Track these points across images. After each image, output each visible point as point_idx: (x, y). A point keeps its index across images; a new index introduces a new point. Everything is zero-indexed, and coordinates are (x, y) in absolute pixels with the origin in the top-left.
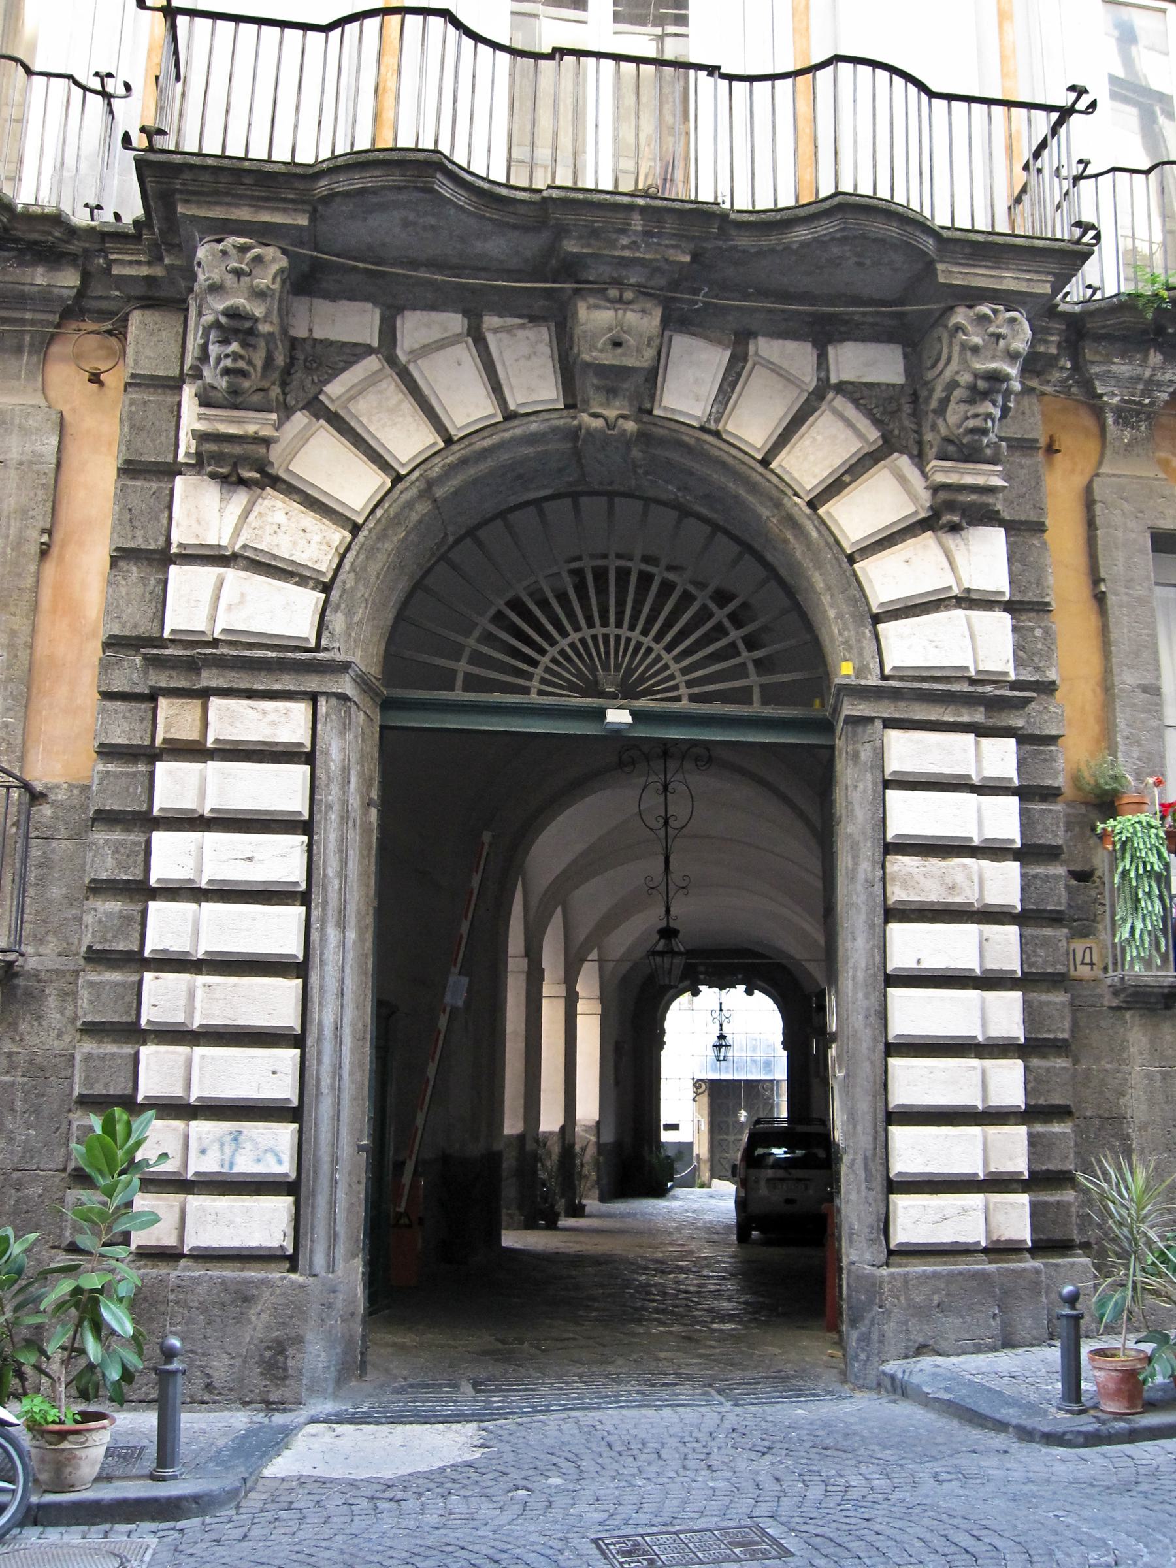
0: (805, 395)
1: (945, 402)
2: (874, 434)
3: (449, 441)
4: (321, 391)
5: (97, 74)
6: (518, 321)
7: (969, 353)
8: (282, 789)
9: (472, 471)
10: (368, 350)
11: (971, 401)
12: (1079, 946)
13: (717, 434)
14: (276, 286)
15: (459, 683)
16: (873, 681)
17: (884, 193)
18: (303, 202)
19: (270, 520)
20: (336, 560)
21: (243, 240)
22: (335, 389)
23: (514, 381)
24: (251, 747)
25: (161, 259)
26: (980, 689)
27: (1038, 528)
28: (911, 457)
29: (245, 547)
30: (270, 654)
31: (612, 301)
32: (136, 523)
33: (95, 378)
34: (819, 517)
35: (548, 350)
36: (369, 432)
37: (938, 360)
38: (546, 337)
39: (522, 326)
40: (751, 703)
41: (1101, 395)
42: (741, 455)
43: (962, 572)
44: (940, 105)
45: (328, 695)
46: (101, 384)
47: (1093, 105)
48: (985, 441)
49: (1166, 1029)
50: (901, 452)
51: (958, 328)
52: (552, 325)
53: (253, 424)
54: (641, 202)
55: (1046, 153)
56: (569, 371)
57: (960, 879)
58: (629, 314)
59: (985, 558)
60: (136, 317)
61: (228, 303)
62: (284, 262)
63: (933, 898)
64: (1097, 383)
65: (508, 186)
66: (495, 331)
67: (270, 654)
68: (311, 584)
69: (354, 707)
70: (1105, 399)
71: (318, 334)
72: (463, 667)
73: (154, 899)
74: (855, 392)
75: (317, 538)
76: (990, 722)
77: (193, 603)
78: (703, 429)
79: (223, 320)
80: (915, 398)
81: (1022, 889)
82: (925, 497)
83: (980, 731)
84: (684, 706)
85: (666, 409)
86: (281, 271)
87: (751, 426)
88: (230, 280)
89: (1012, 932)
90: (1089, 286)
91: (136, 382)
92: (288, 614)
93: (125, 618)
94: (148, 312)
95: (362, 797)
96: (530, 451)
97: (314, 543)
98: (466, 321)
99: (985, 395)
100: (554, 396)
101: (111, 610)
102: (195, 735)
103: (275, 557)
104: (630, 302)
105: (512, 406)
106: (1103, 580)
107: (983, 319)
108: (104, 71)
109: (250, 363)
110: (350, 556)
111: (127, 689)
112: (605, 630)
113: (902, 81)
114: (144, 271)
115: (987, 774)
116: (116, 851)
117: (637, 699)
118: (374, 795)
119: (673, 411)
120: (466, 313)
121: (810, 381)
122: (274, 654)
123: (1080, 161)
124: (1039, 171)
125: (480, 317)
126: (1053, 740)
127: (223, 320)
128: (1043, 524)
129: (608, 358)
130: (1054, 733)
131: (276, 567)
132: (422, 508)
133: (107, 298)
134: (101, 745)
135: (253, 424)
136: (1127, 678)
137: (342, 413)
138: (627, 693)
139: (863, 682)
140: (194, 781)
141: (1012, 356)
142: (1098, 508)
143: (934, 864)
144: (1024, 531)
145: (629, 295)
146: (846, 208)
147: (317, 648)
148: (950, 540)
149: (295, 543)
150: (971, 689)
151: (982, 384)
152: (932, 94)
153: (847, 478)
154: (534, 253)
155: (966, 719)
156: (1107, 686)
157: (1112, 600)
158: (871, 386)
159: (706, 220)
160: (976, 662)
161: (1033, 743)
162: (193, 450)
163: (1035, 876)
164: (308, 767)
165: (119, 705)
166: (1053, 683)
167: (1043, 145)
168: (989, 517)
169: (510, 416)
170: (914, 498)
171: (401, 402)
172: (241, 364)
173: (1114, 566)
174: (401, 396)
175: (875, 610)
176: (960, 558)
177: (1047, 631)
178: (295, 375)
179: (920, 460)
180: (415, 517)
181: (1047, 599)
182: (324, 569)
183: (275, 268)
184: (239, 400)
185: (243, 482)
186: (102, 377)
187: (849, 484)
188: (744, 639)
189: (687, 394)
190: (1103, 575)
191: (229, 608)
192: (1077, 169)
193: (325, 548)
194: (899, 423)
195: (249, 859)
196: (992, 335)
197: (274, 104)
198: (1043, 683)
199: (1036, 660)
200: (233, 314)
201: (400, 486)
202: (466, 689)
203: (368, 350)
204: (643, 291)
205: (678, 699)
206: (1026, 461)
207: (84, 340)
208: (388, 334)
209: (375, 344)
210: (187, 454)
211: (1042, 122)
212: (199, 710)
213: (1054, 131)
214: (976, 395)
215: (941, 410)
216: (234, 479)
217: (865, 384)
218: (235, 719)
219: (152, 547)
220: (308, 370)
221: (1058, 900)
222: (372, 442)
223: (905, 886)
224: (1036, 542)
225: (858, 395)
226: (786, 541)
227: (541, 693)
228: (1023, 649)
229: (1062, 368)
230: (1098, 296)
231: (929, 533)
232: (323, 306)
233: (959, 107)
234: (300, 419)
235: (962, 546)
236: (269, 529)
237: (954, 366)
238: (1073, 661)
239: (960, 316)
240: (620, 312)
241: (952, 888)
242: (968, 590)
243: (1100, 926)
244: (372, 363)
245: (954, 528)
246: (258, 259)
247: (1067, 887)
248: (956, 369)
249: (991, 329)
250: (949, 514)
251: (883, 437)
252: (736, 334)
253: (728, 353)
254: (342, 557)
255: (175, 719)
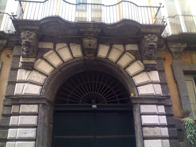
0: (122, 52)
1: (145, 51)
2: (134, 57)
3: (64, 62)
4: (43, 56)
5: (11, 13)
6: (75, 44)
7: (148, 42)
8: (32, 120)
9: (68, 67)
10: (51, 49)
11: (149, 50)
12: (181, 143)
13: (108, 59)
14: (34, 38)
15: (67, 102)
16: (137, 96)
17: (131, 18)
18: (38, 25)
19: (33, 75)
20: (44, 81)
21: (28, 31)
22: (45, 55)
23: (74, 53)
24: (27, 113)
25: (18, 38)
26: (156, 97)
27: (164, 71)
28: (140, 61)
29: (29, 80)
30: (31, 97)
31: (89, 39)
32: (12, 77)
33: (8, 56)
34: (126, 71)
35: (80, 48)
36: (50, 61)
37: (143, 44)
38: (80, 46)
39: (76, 45)
40: (117, 103)
41: (172, 50)
42: (111, 61)
43: (151, 78)
44: (139, 8)
45: (41, 103)
46: (9, 57)
47: (163, 7)
48: (152, 56)
49: (194, 56)
50: (139, 60)
51: (145, 38)
52: (81, 45)
53: (32, 60)
54: (92, 23)
55: (157, 15)
56: (83, 50)
57: (156, 131)
58: (92, 40)
59: (155, 76)
60: (15, 47)
61: (26, 40)
62: (35, 34)
63: (152, 135)
64: (171, 49)
65: (71, 22)
66: (72, 45)
67: (31, 97)
68: (40, 85)
69: (46, 105)
70: (172, 51)
71: (43, 47)
72: (68, 100)
73: (8, 141)
74: (131, 52)
75: (41, 78)
76: (159, 103)
77: (20, 89)
78: (105, 58)
79: (25, 43)
80: (140, 52)
81: (169, 133)
82: (143, 66)
83: (157, 104)
84: (106, 104)
85: (99, 55)
86: (35, 36)
87: (113, 57)
88: (26, 37)
89: (168, 141)
90: (167, 33)
91: (14, 56)
92: (35, 90)
93: (8, 93)
94: (17, 46)
95: (48, 122)
96: (78, 63)
97: (40, 79)
98: (67, 45)
99: (152, 48)
100: (81, 54)
101: (7, 92)
102: (18, 111)
103: (34, 81)
104: (92, 39)
105: (74, 56)
106: (176, 79)
107: (149, 37)
108: (12, 12)
109: (30, 50)
110: (46, 80)
111: (8, 104)
112: (92, 92)
113: (133, 4)
114: (16, 40)
115: (159, 112)
116: (3, 133)
117: (98, 103)
118: (52, 122)
119: (100, 56)
120: (67, 43)
121: (123, 50)
122: (32, 97)
123: (163, 16)
124: (157, 19)
125: (69, 44)
126: (171, 106)
127: (25, 43)
128: (164, 70)
129: (89, 47)
130: (171, 104)
131: (34, 83)
132: (60, 73)
133: (11, 44)
134: (2, 114)
135: (32, 60)
136: (183, 95)
137: (46, 59)
138: (97, 102)
139: (135, 97)
140: (17, 119)
141: (155, 42)
142: (173, 68)
143: (151, 129)
144: (161, 72)
145: (91, 37)
146: (124, 21)
147: (40, 96)
148: (149, 73)
149: (37, 79)
150: (155, 97)
151: (150, 47)
152: (138, 6)
153: (130, 64)
154: (77, 33)
155: (154, 102)
156: (180, 96)
157: (178, 82)
158: (133, 50)
159: (102, 26)
160: (155, 93)
161: (168, 107)
162: (21, 65)
163: (171, 130)
164: (37, 116)
165: (7, 107)
166: (170, 96)
167: (157, 14)
168: (155, 70)
169: (74, 58)
170: (142, 67)
171: (56, 57)
172: (28, 50)
173: (177, 76)
174: (56, 56)
175: (136, 85)
176: (150, 76)
177: (167, 88)
178: (39, 53)
179: (142, 61)
180: (58, 74)
181: (167, 82)
182: (42, 83)
183: (33, 35)
184: (28, 56)
185: (29, 70)
186: (9, 56)
187: (130, 65)
188: (118, 96)
189: (103, 52)
190: (176, 78)
191: (25, 90)
192: (162, 18)
193: (42, 79)
194: (138, 56)
195: (25, 133)
196: (151, 39)
197: (35, 13)
198: (168, 96)
199: (166, 92)
200: (26, 42)
201: (55, 69)
202: (68, 103)
203: (51, 49)
204: (94, 37)
205: (105, 103)
206: (160, 61)
207: (8, 51)
208: (55, 47)
209: (52, 48)
210: (20, 66)
211: (156, 10)
212: (19, 107)
213: (158, 11)
214: (150, 49)
215: (144, 52)
216: (28, 69)
217: (132, 50)
218: (25, 108)
219: (14, 81)
220: (41, 52)
221: (176, 135)
222: (51, 63)
223: (146, 133)
224: (163, 73)
225: (130, 52)
226: (120, 75)
227: (81, 103)
228: (163, 91)
229: (164, 47)
230: (168, 35)
231: (145, 72)
232: (44, 43)
233: (142, 8)
234: (39, 60)
235: (150, 74)
236: (33, 77)
237: (145, 45)
238: (173, 92)
239: (146, 37)
240: (90, 40)
241: (155, 133)
242: (152, 81)
243: (185, 139)
244: (51, 51)
245: (149, 71)
246: (31, 34)
247: (177, 132)
248: (146, 45)
249: (151, 38)
250: (147, 69)
251: (135, 58)
252: (110, 44)
253: (109, 47)
254: (45, 81)
255: (14, 109)
